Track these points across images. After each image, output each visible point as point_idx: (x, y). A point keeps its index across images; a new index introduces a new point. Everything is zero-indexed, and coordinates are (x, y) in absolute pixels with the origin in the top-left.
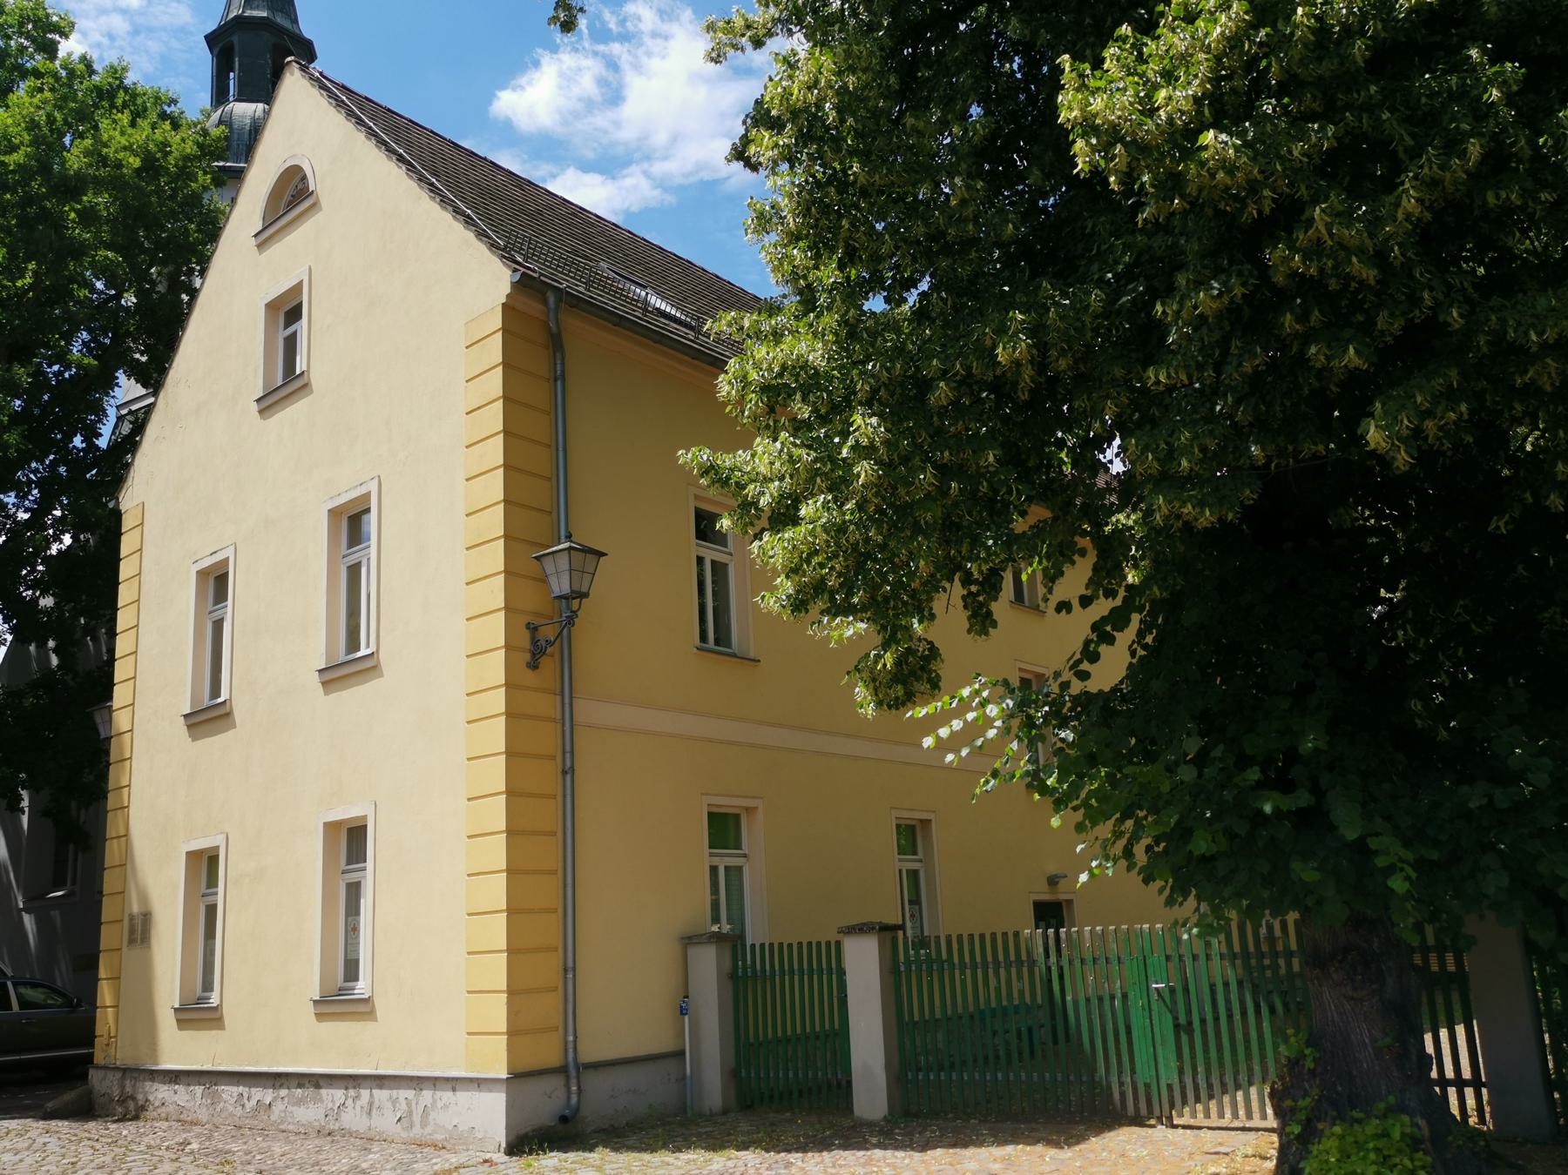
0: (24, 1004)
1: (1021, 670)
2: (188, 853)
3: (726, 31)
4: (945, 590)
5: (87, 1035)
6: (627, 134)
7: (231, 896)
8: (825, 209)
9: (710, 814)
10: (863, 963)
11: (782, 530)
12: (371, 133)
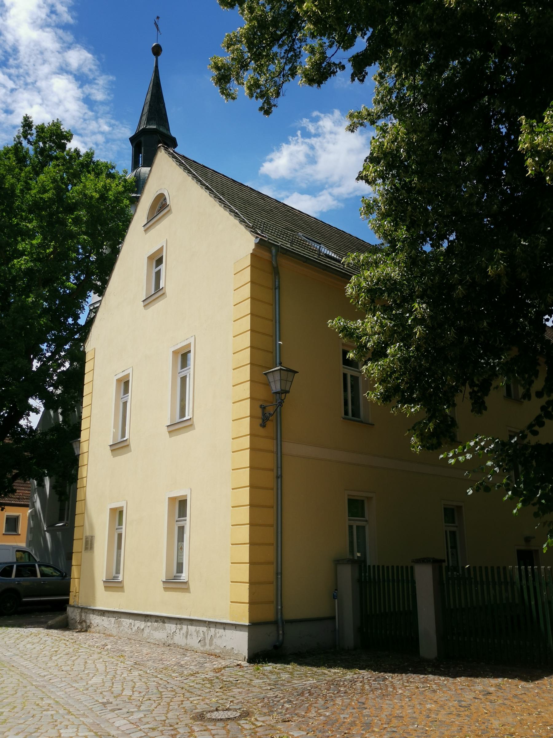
0: (43, 574)
1: (510, 431)
2: (111, 509)
3: (358, 117)
4: (461, 391)
5: (66, 591)
6: (320, 176)
7: (128, 529)
8: (400, 202)
9: (349, 500)
10: (424, 577)
11: (378, 361)
12: (194, 177)
